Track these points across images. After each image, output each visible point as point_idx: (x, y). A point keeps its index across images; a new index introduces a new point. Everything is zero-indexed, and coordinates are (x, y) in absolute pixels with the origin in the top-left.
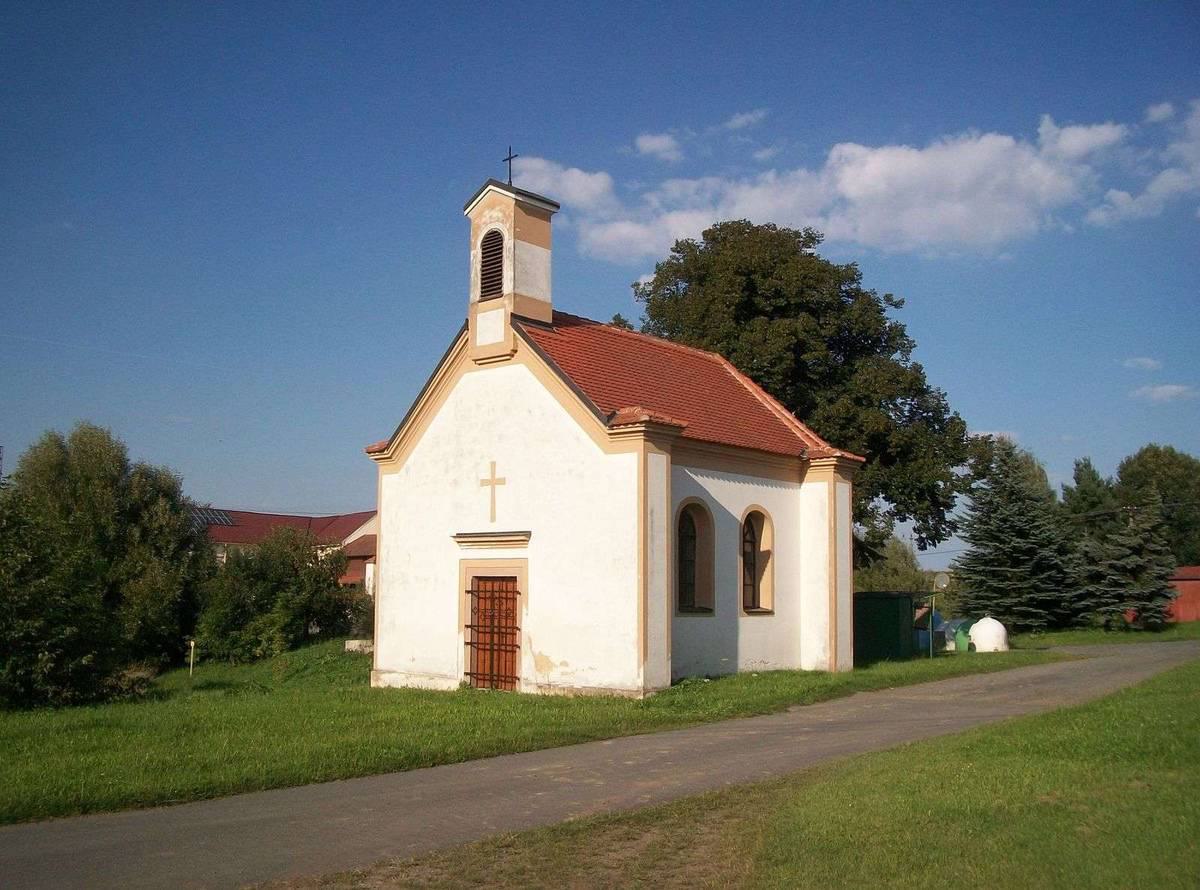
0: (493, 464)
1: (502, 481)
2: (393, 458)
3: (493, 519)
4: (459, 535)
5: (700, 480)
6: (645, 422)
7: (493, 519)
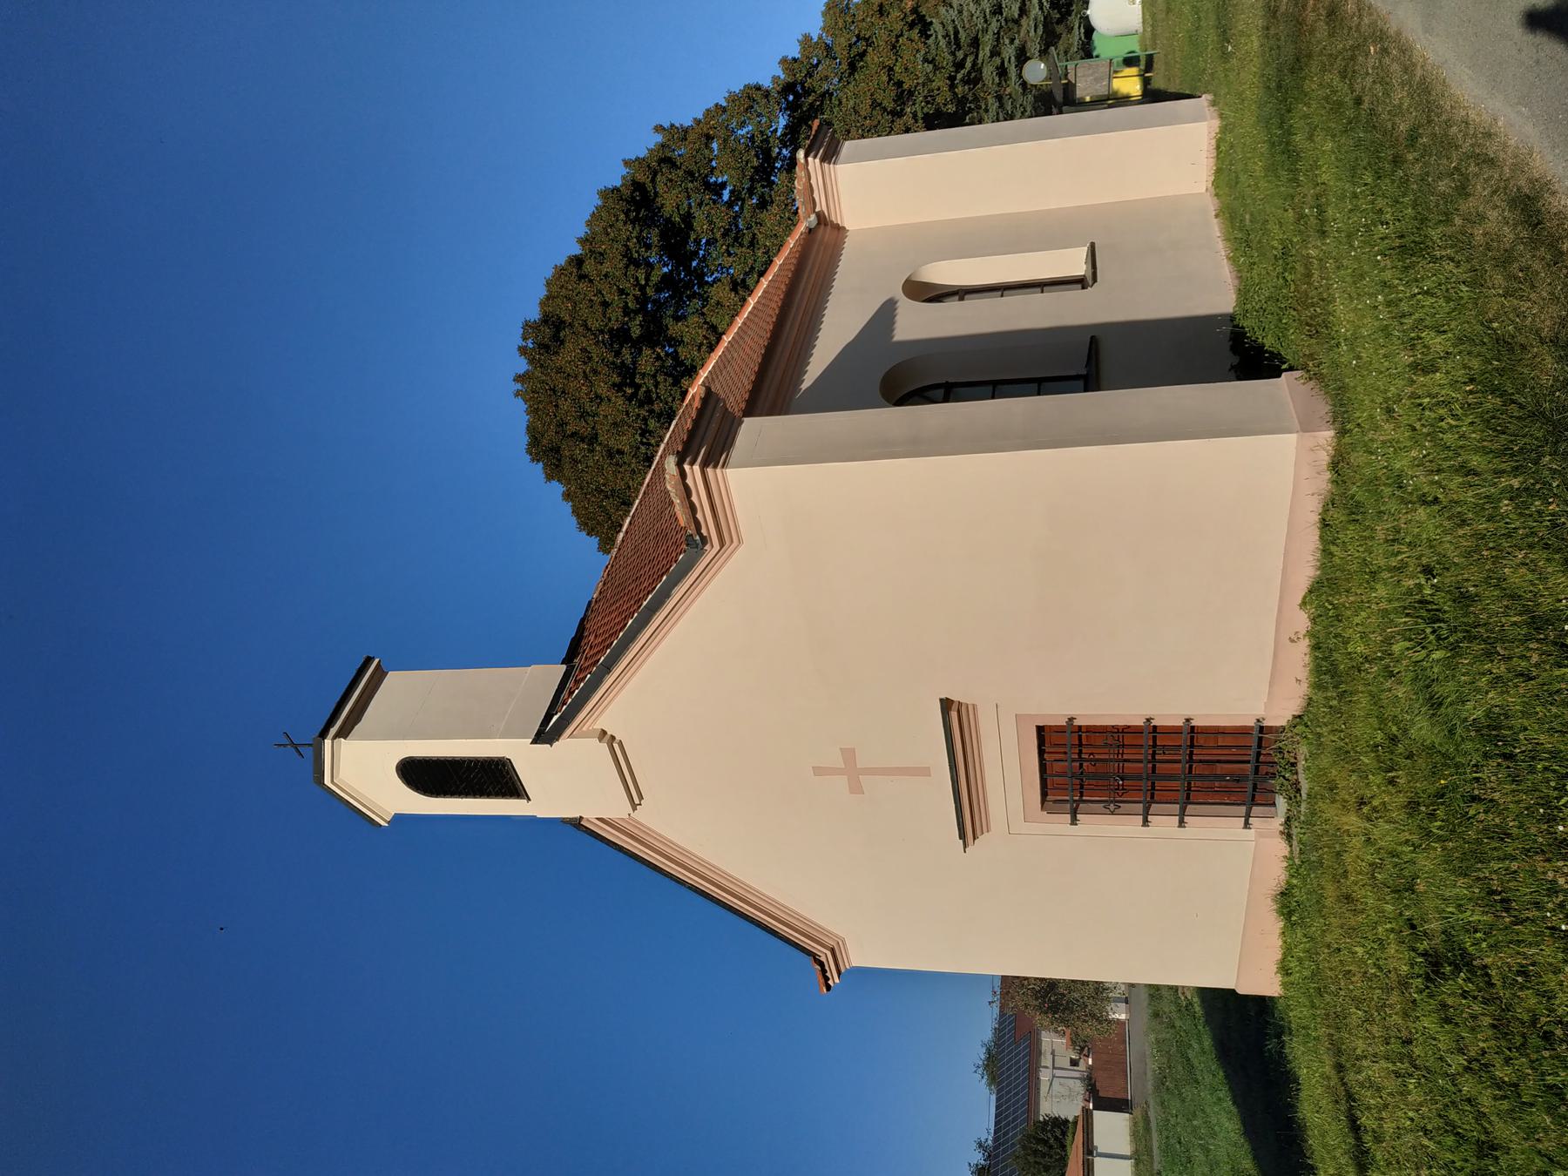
0: (818, 771)
1: (849, 754)
2: (832, 943)
3: (924, 772)
4: (962, 835)
5: (804, 386)
6: (680, 464)
7: (924, 772)
